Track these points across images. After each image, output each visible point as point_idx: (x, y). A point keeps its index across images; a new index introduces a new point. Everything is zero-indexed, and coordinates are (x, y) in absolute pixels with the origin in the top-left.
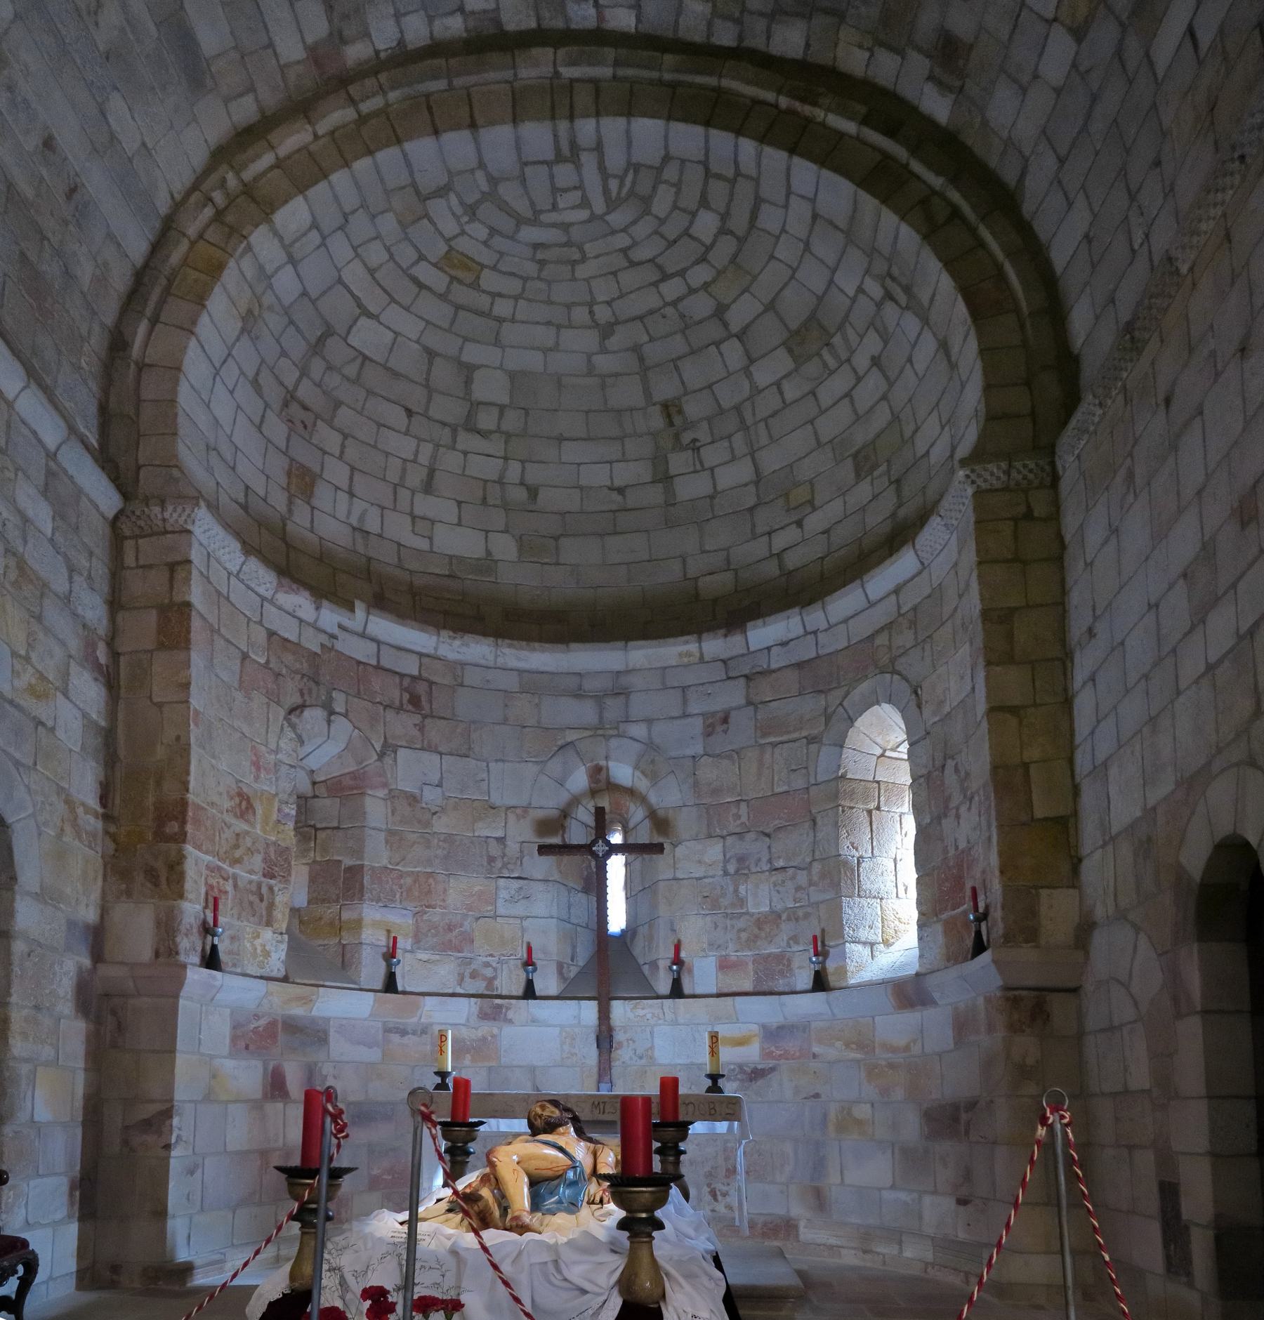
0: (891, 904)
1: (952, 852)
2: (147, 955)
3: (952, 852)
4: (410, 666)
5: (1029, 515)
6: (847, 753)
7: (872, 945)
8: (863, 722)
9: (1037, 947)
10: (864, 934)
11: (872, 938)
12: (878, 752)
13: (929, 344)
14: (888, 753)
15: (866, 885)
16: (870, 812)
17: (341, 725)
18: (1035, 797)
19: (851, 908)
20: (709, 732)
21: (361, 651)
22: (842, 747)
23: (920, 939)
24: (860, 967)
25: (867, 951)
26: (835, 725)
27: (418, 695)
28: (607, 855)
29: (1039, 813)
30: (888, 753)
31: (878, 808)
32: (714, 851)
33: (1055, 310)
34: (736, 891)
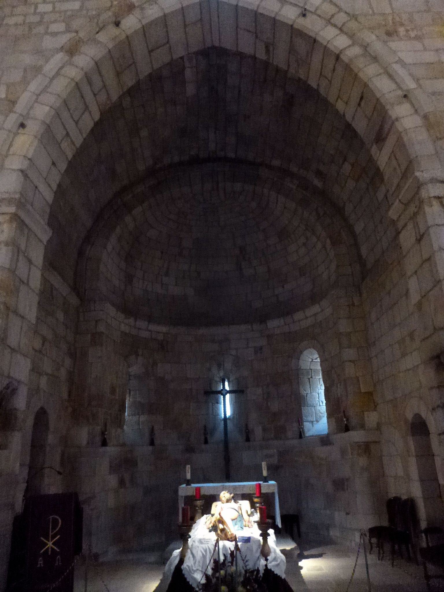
0: (318, 408)
1: (336, 396)
2: (84, 442)
3: (336, 396)
4: (161, 337)
5: (353, 305)
6: (301, 361)
7: (312, 422)
8: (305, 353)
9: (365, 430)
10: (310, 419)
11: (312, 420)
12: (310, 360)
13: (319, 245)
14: (314, 360)
15: (309, 402)
16: (309, 379)
17: (140, 359)
18: (361, 386)
19: (305, 410)
20: (256, 352)
21: (144, 334)
22: (299, 359)
23: (328, 422)
24: (309, 430)
25: (311, 425)
26: (296, 354)
27: (163, 346)
28: (226, 394)
29: (363, 391)
30: (314, 360)
31: (312, 377)
32: (259, 391)
33: (356, 245)
34: (267, 404)
